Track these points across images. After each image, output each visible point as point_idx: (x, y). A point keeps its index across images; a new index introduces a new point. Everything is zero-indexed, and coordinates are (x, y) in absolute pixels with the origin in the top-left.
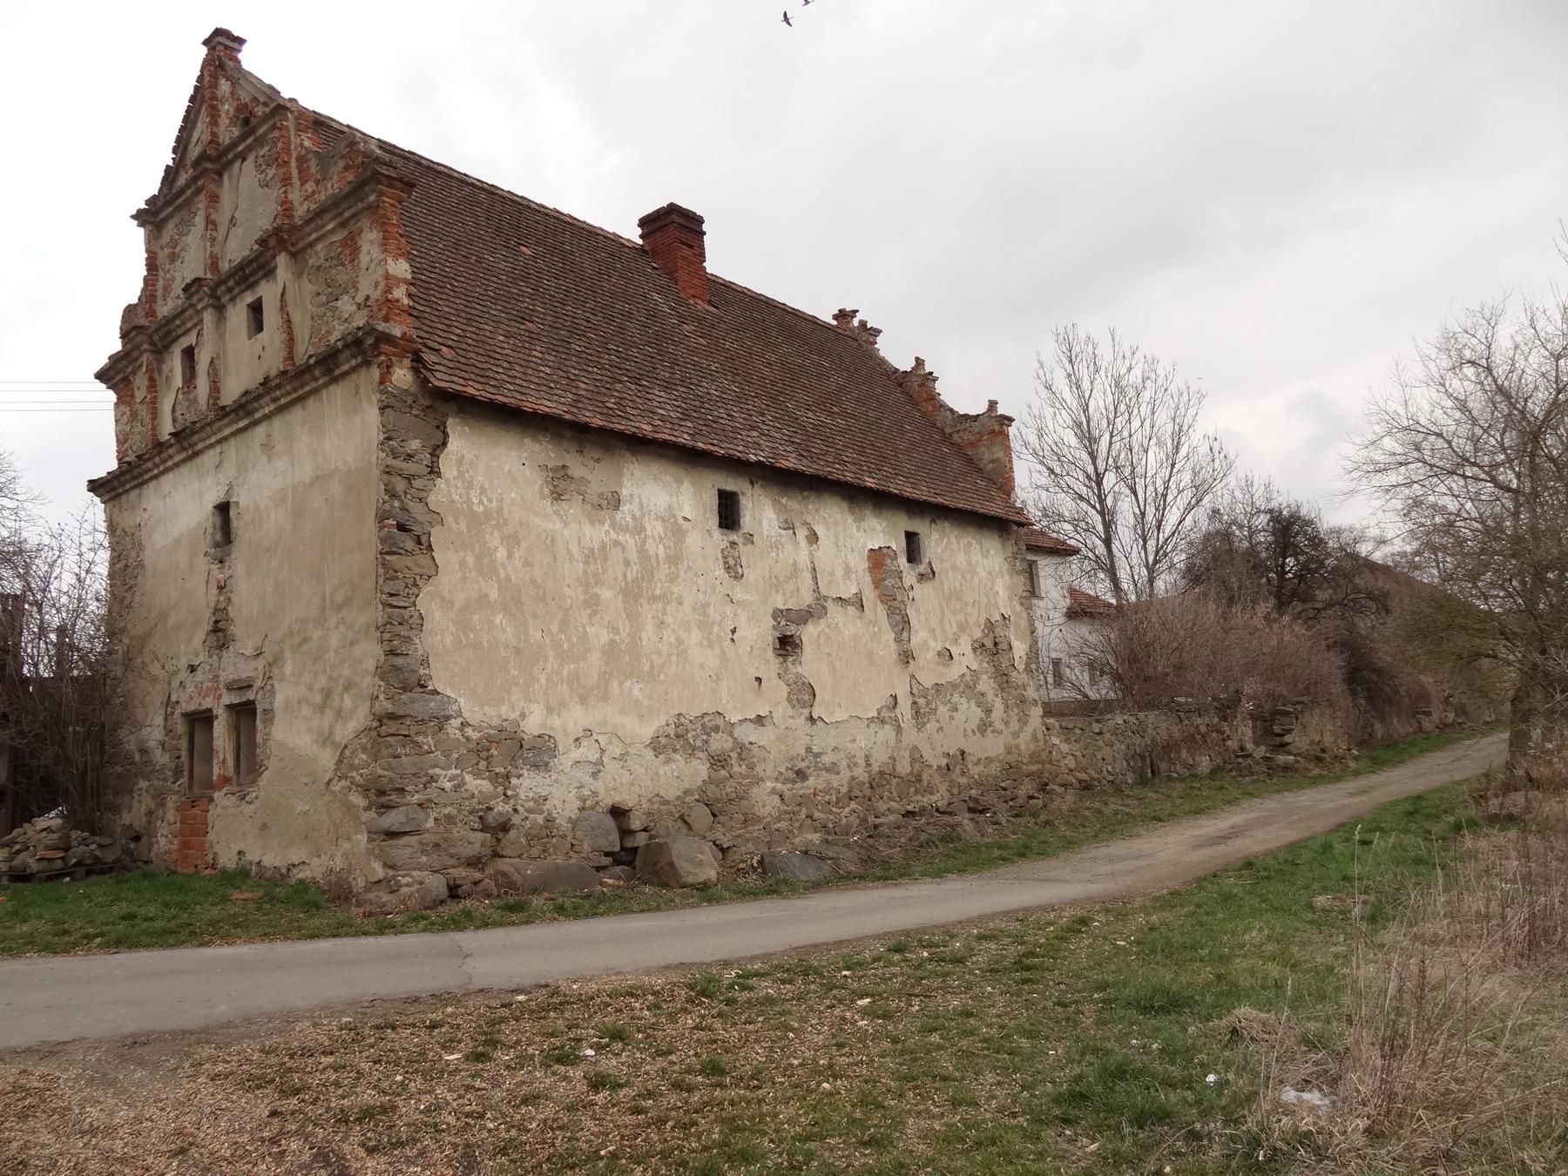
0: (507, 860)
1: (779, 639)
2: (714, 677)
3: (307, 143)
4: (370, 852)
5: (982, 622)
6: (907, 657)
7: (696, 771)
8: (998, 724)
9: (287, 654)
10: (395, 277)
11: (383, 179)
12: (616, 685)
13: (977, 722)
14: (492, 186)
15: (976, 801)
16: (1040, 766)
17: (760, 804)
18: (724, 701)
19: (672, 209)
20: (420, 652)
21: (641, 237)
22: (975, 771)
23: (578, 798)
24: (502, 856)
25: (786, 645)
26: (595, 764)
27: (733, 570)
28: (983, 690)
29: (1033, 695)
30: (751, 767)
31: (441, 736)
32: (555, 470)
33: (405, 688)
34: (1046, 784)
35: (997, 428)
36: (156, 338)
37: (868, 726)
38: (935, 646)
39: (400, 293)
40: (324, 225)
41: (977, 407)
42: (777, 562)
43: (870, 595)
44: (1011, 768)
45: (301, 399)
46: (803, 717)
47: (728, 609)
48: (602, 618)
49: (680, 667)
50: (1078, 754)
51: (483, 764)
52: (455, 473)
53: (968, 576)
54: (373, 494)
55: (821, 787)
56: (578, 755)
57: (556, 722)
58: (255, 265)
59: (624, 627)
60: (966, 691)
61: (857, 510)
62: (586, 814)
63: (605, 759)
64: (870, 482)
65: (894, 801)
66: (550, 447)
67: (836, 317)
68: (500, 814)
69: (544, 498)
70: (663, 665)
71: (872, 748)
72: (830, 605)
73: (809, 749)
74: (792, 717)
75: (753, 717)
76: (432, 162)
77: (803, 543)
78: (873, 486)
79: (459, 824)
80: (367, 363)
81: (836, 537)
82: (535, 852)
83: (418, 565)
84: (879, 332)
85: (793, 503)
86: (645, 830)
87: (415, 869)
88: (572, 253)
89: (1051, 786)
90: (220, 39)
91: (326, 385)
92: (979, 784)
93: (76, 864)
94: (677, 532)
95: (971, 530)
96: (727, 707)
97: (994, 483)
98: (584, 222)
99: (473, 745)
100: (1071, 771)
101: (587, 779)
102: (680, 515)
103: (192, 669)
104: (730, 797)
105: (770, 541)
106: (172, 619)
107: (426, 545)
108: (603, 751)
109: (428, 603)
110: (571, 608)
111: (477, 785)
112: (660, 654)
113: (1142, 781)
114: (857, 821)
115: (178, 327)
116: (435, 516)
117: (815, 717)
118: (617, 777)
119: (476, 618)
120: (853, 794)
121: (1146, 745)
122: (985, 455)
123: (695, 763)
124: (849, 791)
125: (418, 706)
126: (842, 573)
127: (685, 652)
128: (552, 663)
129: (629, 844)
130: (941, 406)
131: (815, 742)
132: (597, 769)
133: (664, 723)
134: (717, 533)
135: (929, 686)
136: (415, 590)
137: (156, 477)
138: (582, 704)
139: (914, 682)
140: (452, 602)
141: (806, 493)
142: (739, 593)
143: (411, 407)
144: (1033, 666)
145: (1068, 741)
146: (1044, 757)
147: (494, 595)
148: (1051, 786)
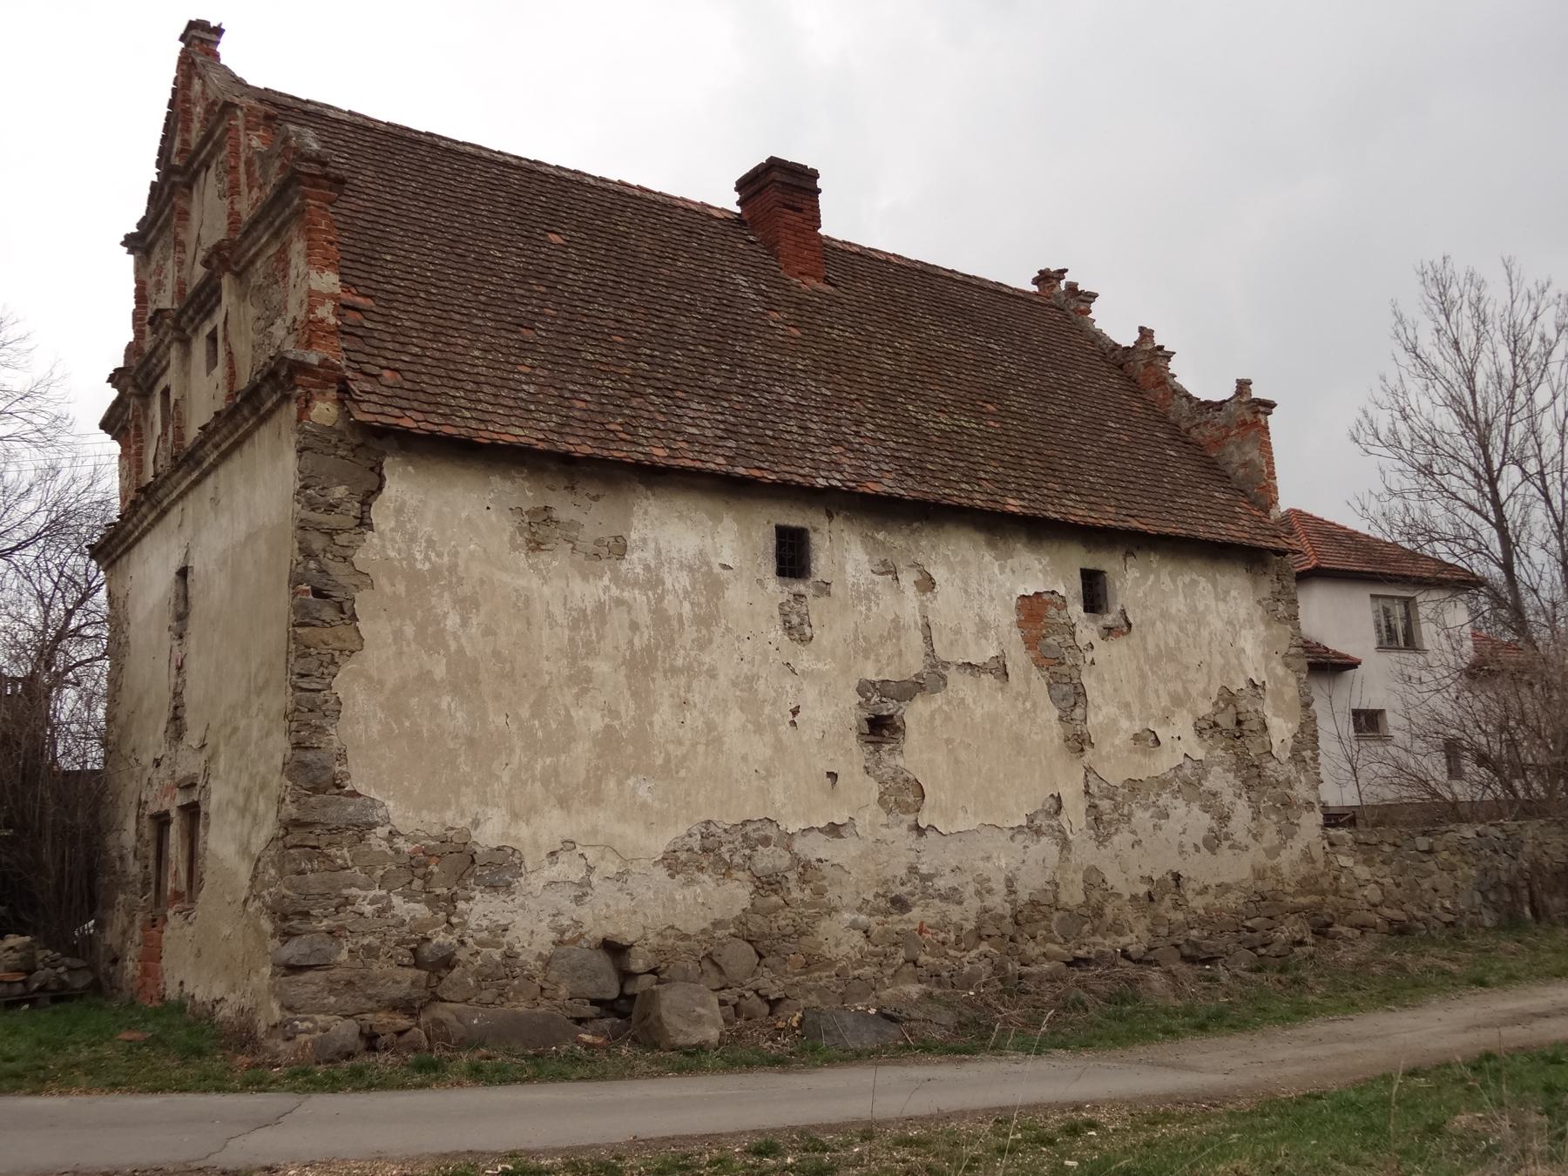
0: (448, 1005)
1: (869, 721)
2: (763, 772)
3: (255, 143)
4: (272, 989)
5: (1214, 692)
6: (1079, 743)
7: (735, 896)
8: (1241, 836)
9: (222, 748)
10: (319, 293)
11: (305, 178)
12: (612, 784)
13: (1204, 833)
14: (535, 162)
15: (1196, 945)
16: (1316, 898)
17: (832, 942)
18: (778, 805)
19: (774, 164)
20: (335, 745)
21: (739, 203)
22: (1198, 903)
23: (554, 929)
24: (443, 1000)
25: (880, 729)
26: (580, 885)
27: (797, 631)
28: (1214, 789)
29: (1306, 795)
30: (820, 892)
31: (362, 848)
32: (533, 513)
33: (316, 790)
34: (1329, 925)
35: (1249, 418)
36: (139, 380)
37: (1012, 838)
38: (1129, 727)
39: (325, 312)
40: (260, 238)
41: (1221, 391)
42: (867, 617)
43: (1018, 658)
44: (1264, 899)
45: (237, 445)
46: (905, 826)
47: (788, 682)
48: (594, 697)
49: (710, 761)
50: (1388, 881)
51: (418, 884)
52: (392, 524)
53: (1191, 628)
54: (289, 551)
55: (932, 922)
56: (555, 874)
57: (523, 831)
58: (208, 290)
59: (628, 708)
60: (1185, 789)
61: (1000, 544)
62: (563, 949)
63: (594, 879)
64: (1013, 505)
65: (1056, 943)
66: (527, 484)
67: (1036, 281)
68: (439, 946)
69: (515, 548)
70: (685, 758)
71: (1018, 869)
72: (952, 675)
73: (913, 870)
74: (887, 826)
75: (822, 825)
76: (457, 142)
77: (910, 590)
78: (1016, 510)
79: (383, 958)
80: (286, 398)
81: (965, 581)
82: (487, 996)
83: (338, 638)
84: (1094, 296)
85: (896, 540)
86: (653, 972)
87: (319, 1013)
88: (626, 235)
89: (1337, 928)
90: (194, 32)
91: (257, 426)
92: (1203, 922)
93: (41, 989)
94: (711, 583)
95: (1196, 563)
96: (783, 812)
97: (1247, 495)
98: (660, 194)
99: (405, 860)
100: (1375, 906)
101: (566, 904)
102: (715, 562)
103: (157, 763)
104: (785, 932)
105: (858, 592)
106: (146, 705)
107: (349, 613)
108: (590, 869)
109: (347, 684)
110: (549, 686)
111: (409, 909)
112: (680, 743)
113: (1511, 923)
114: (990, 969)
115: (156, 365)
116: (364, 578)
117: (923, 825)
118: (611, 903)
119: (414, 701)
120: (984, 932)
121: (1521, 871)
122: (1236, 455)
123: (731, 886)
124: (978, 928)
125: (332, 811)
126: (974, 630)
127: (719, 740)
128: (518, 757)
129: (629, 990)
130: (1175, 391)
131: (923, 860)
132: (582, 891)
133: (684, 832)
134: (773, 583)
135: (1119, 784)
136: (332, 669)
137: (138, 540)
138: (562, 807)
139: (1091, 777)
140: (381, 682)
141: (915, 525)
142: (805, 659)
143: (336, 446)
144: (1308, 754)
145: (1368, 862)
146: (1326, 886)
147: (440, 671)
148: (1337, 928)
